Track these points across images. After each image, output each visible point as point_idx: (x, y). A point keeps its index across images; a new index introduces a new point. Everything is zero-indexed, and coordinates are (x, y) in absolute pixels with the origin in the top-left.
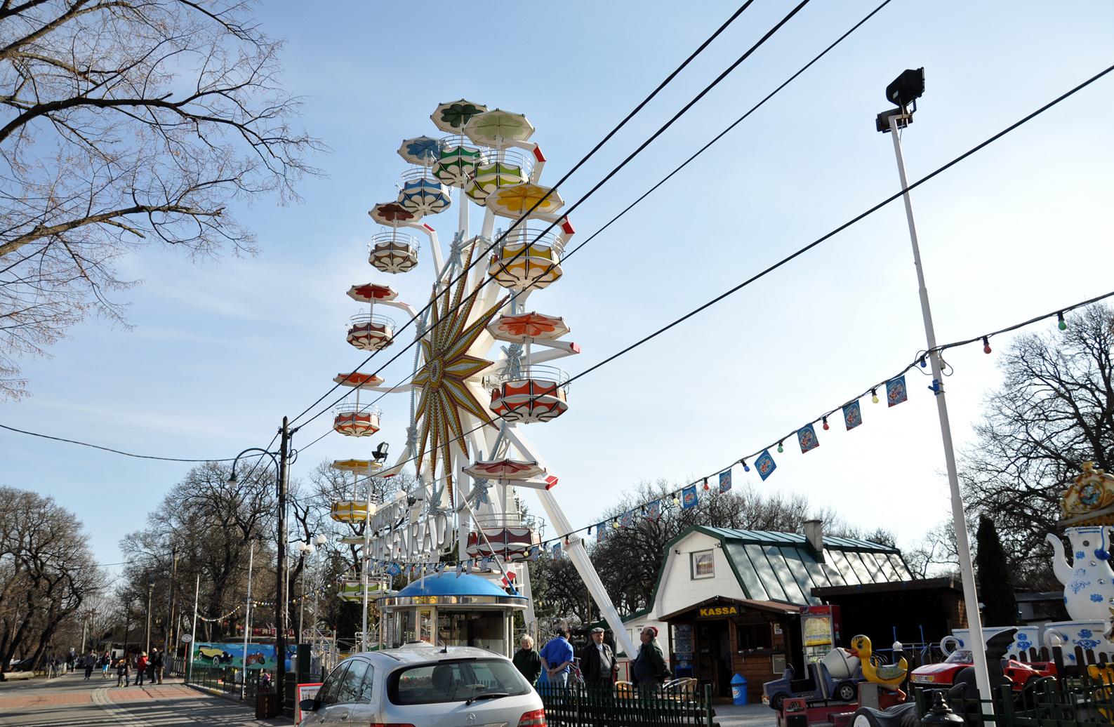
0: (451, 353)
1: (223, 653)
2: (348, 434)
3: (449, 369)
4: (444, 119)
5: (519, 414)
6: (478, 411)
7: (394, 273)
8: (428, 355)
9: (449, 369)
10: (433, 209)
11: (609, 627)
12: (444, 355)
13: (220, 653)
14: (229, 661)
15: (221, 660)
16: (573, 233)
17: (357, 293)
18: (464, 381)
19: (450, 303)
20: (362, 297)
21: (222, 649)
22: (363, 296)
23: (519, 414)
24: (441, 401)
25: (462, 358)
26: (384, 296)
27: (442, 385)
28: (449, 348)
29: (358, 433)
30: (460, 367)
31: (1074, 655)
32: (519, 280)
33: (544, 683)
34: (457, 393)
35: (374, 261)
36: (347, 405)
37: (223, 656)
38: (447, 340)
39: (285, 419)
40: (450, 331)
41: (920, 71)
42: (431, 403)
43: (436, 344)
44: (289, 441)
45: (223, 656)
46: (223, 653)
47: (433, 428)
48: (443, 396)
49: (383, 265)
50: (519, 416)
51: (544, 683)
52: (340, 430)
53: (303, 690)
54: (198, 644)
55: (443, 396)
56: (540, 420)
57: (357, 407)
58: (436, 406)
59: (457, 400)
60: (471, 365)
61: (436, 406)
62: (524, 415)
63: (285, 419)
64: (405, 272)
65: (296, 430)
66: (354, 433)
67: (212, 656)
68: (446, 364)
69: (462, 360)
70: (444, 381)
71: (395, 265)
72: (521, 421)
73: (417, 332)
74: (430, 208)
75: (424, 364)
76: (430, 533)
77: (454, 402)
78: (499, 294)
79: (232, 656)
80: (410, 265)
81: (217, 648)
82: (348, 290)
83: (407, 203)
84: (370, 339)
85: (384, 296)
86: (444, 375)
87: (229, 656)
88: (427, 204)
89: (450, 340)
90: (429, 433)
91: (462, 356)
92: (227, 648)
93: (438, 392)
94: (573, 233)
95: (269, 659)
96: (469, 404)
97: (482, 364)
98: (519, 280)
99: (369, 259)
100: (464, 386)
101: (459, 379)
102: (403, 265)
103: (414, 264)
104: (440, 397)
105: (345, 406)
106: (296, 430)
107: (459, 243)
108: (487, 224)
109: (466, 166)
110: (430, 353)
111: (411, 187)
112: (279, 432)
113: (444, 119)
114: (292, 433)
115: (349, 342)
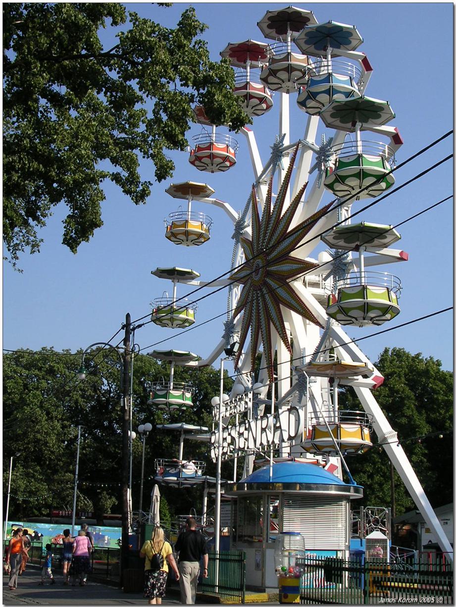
0: (274, 253)
1: (34, 532)
2: (164, 325)
3: (273, 268)
4: (269, 27)
5: (354, 318)
6: (307, 314)
7: (213, 172)
8: (249, 252)
9: (273, 268)
10: (255, 112)
11: (424, 520)
12: (268, 254)
14: (39, 539)
16: (402, 143)
17: (175, 191)
20: (179, 194)
21: (33, 528)
22: (180, 193)
23: (354, 318)
25: (286, 259)
27: (265, 284)
28: (274, 247)
30: (285, 267)
32: (208, 166)
33: (322, 557)
34: (281, 292)
35: (194, 161)
36: (165, 299)
39: (128, 316)
41: (3, 3)
46: (34, 532)
47: (254, 323)
49: (203, 165)
50: (353, 320)
51: (322, 557)
52: (157, 322)
54: (11, 523)
56: (373, 323)
59: (280, 299)
60: (295, 266)
62: (358, 319)
63: (128, 316)
65: (140, 326)
66: (170, 325)
68: (269, 263)
69: (286, 261)
70: (268, 280)
71: (215, 165)
72: (356, 325)
73: (235, 230)
75: (244, 261)
76: (280, 426)
77: (277, 300)
78: (263, 193)
79: (42, 535)
80: (229, 165)
82: (167, 189)
86: (269, 274)
87: (40, 535)
88: (250, 107)
89: (274, 238)
90: (250, 329)
91: (285, 257)
92: (37, 528)
94: (402, 143)
96: (293, 302)
97: (308, 267)
98: (208, 166)
99: (189, 159)
101: (284, 279)
102: (221, 165)
104: (263, 296)
105: (163, 299)
106: (140, 326)
107: (280, 147)
109: (279, 72)
111: (306, 98)
112: (123, 328)
113: (269, 27)
114: (134, 329)
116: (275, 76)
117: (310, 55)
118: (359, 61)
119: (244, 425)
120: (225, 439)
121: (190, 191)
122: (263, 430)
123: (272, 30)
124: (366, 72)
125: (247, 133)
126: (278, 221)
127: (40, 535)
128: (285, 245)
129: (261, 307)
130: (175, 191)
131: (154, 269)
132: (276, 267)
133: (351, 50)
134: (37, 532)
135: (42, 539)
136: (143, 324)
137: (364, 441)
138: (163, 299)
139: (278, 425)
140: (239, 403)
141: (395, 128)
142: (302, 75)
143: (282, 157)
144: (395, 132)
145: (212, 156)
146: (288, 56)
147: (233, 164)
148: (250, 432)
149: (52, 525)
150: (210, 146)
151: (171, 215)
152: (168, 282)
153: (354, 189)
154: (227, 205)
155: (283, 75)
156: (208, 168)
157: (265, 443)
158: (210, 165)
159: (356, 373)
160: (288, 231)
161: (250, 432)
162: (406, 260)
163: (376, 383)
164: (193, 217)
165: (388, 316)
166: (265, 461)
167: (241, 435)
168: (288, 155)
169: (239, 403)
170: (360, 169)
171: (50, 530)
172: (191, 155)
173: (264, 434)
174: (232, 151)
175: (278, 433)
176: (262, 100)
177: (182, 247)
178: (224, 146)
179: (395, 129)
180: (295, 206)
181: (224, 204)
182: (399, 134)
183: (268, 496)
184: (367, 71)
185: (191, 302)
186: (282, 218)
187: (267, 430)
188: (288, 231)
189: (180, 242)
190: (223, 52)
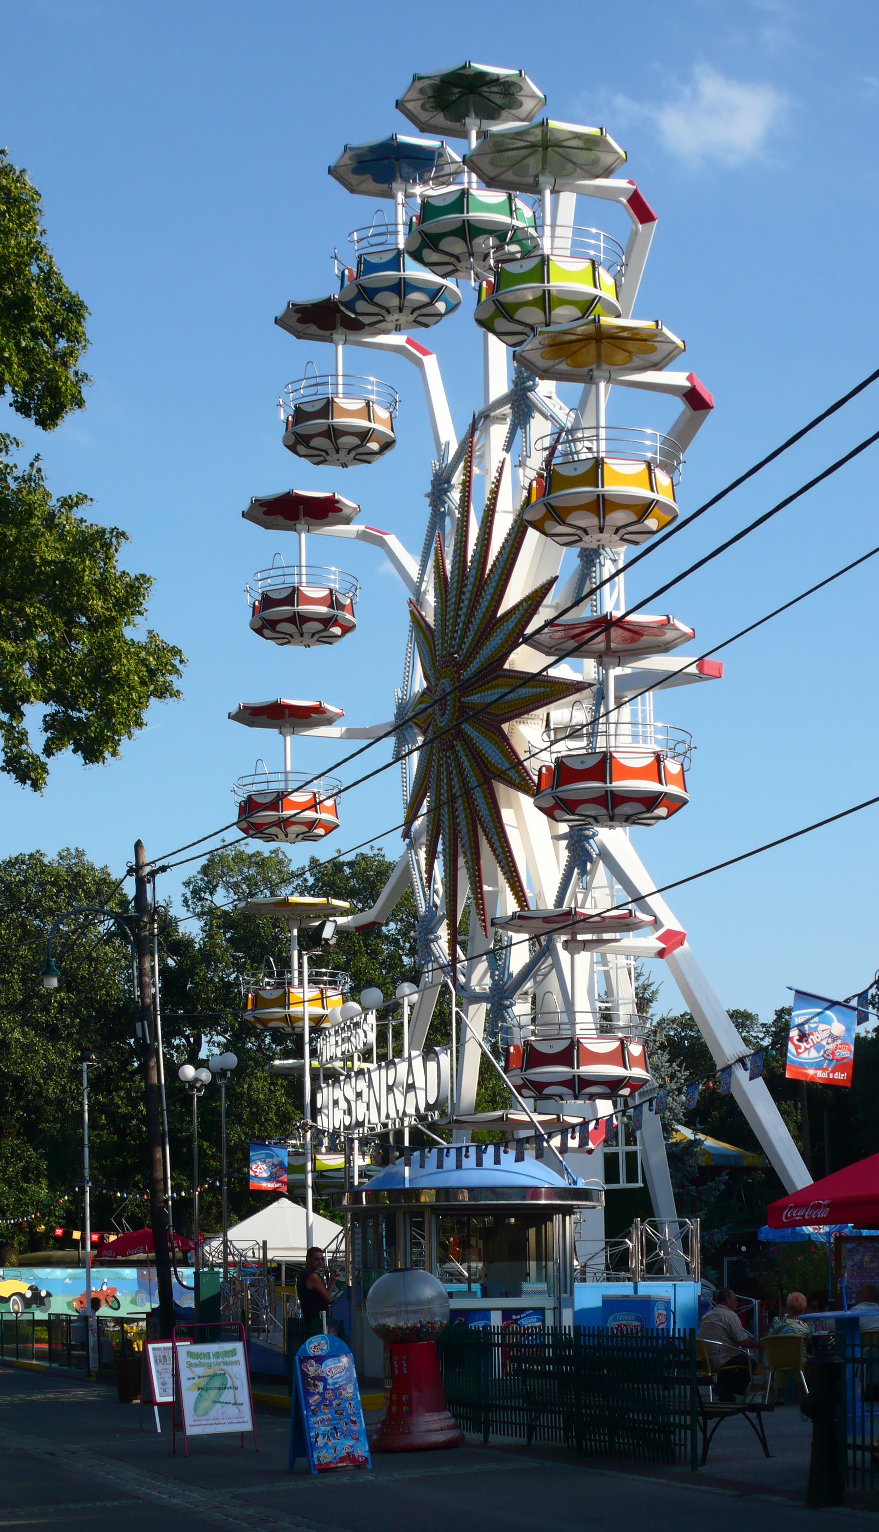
1: (31, 1288)
3: (475, 699)
7: (345, 465)
9: (475, 699)
12: (461, 666)
13: (24, 1288)
15: (28, 1303)
17: (265, 513)
18: (505, 727)
19: (470, 553)
20: (313, 329)
21: (27, 1280)
24: (459, 766)
25: (499, 676)
26: (330, 514)
27: (460, 734)
29: (292, 836)
31: (781, 1335)
37: (29, 1294)
38: (466, 629)
40: (471, 615)
42: (439, 773)
43: (444, 634)
44: (149, 887)
45: (29, 1294)
46: (31, 1288)
48: (462, 753)
53: (153, 1349)
55: (462, 753)
57: (286, 781)
58: (452, 780)
61: (452, 780)
63: (138, 845)
64: (369, 462)
67: (7, 1296)
68: (465, 688)
74: (412, 318)
76: (414, 1082)
79: (49, 1295)
81: (16, 1278)
83: (362, 306)
84: (302, 624)
85: (330, 514)
86: (463, 712)
87: (43, 1294)
89: (473, 627)
90: (440, 842)
92: (36, 1278)
93: (452, 747)
95: (129, 1299)
100: (505, 739)
102: (360, 450)
103: (347, 629)
104: (457, 759)
106: (163, 869)
108: (188, 1277)
110: (434, 662)
115: (288, 447)
116: (437, 249)
117: (516, 190)
118: (620, 202)
119: (362, 1076)
120: (336, 1102)
121: (301, 512)
122: (390, 1089)
123: (365, 177)
124: (640, 226)
125: (421, 360)
126: (481, 583)
127: (43, 1294)
128: (494, 643)
129: (457, 787)
130: (265, 513)
131: (234, 709)
132: (479, 695)
133: (597, 177)
134: (37, 1289)
135: (50, 1302)
136: (168, 867)
137: (629, 1071)
138: (258, 779)
139: (410, 1082)
140: (354, 1032)
141: (687, 374)
142: (429, 301)
143: (530, 395)
144: (688, 384)
145: (334, 433)
146: (462, 200)
147: (387, 445)
148: (371, 1091)
149: (70, 1271)
150: (327, 408)
151: (259, 576)
152: (268, 735)
153: (587, 534)
154: (391, 540)
155: (456, 246)
156: (328, 458)
157: (393, 1114)
158: (332, 452)
159: (628, 925)
160: (498, 615)
161: (371, 1091)
162: (717, 677)
163: (664, 946)
164: (312, 578)
165: (662, 811)
166: (449, 1122)
167: (359, 1095)
168: (505, 419)
169: (354, 1032)
170: (598, 495)
171: (67, 1281)
172: (287, 430)
173: (391, 1096)
174: (383, 414)
175: (411, 1095)
176: (436, 293)
177: (294, 651)
178: (359, 405)
179: (690, 378)
180: (514, 551)
181: (385, 537)
182: (698, 388)
183: (404, 1213)
184: (641, 223)
185: (303, 783)
186: (489, 575)
187: (395, 1089)
188: (498, 615)
189: (285, 639)
190: (336, 167)
